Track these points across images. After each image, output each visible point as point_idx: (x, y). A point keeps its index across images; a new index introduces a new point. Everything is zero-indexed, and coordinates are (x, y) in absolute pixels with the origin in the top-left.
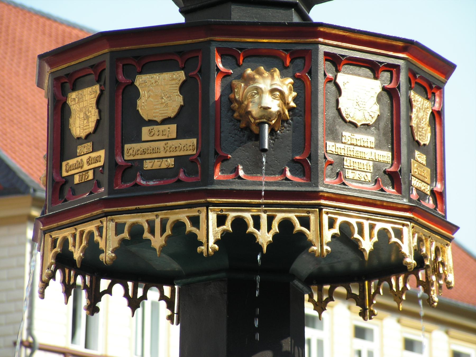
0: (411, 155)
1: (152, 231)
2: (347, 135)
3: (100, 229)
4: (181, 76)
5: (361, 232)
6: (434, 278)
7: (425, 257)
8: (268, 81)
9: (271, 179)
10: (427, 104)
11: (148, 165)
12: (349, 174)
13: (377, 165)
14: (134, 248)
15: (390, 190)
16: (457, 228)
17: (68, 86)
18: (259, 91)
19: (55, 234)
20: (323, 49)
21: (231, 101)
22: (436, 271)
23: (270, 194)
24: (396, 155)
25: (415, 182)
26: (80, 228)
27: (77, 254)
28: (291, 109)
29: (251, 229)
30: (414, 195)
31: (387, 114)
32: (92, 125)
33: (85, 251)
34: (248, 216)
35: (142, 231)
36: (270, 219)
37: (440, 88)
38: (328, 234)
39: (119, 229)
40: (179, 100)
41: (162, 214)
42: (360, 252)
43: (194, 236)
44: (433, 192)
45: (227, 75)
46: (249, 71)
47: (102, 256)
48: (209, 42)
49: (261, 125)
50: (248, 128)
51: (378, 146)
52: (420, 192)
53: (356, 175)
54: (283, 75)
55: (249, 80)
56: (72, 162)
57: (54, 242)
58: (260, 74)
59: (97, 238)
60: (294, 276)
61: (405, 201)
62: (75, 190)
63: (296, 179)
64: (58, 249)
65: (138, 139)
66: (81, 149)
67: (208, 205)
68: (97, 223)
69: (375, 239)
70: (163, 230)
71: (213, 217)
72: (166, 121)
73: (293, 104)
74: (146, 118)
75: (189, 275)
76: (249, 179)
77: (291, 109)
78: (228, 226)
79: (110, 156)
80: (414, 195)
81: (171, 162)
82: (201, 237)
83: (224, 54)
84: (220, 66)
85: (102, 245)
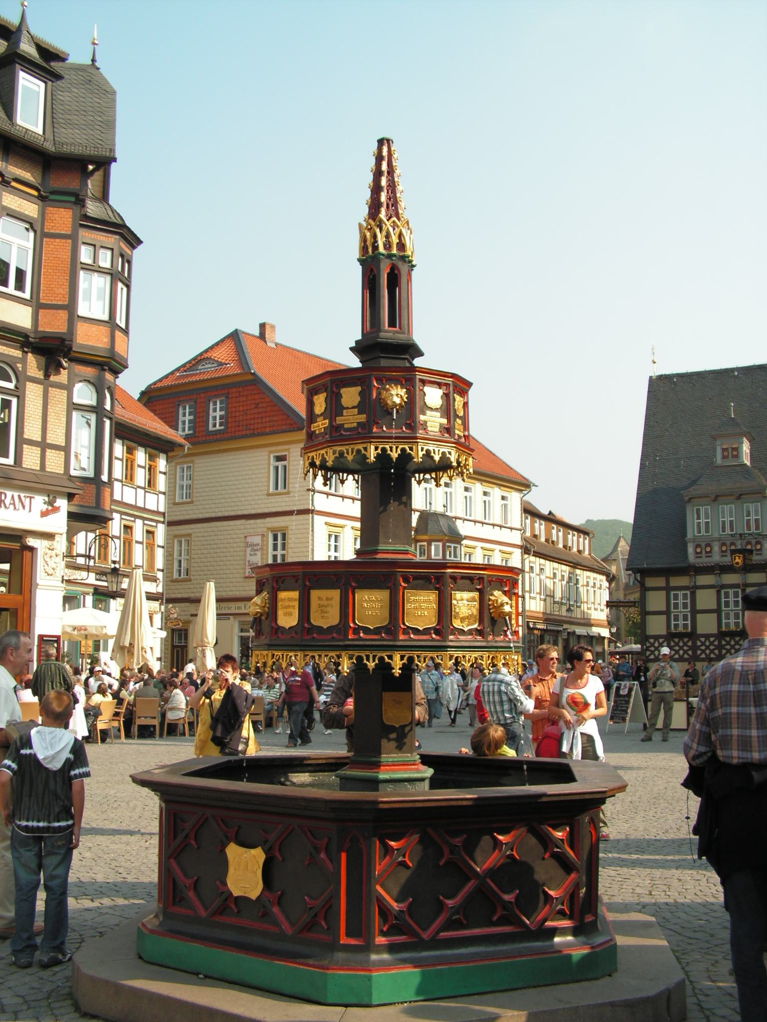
0: (455, 420)
1: (348, 453)
2: (428, 413)
3: (326, 453)
4: (359, 388)
5: (434, 453)
6: (465, 471)
7: (461, 462)
8: (395, 391)
9: (397, 431)
10: (462, 399)
11: (346, 426)
12: (429, 429)
13: (441, 425)
14: (342, 460)
15: (447, 435)
16: (140, 242)
17: (314, 393)
18: (392, 395)
19: (309, 454)
20: (418, 377)
21: (380, 399)
22: (465, 468)
23: (396, 438)
24: (449, 421)
25: (457, 432)
26: (319, 452)
27: (318, 463)
28: (405, 402)
29: (389, 452)
30: (456, 437)
31: (445, 404)
32: (323, 409)
33: (321, 461)
34: (388, 447)
35: (344, 453)
36: (397, 448)
37: (467, 392)
38: (421, 454)
39: (334, 453)
40: (359, 399)
41: (352, 446)
42: (435, 461)
43: (365, 455)
44: (464, 436)
45: (378, 388)
46: (388, 386)
47: (327, 464)
48: (371, 375)
49: (392, 409)
50: (387, 410)
51: (441, 417)
52: (460, 437)
53: (433, 429)
54: (402, 388)
55: (387, 390)
56: (315, 424)
57: (309, 457)
58: (392, 387)
59: (325, 456)
60: (407, 471)
61: (453, 440)
62: (317, 436)
63: (408, 431)
64: (310, 461)
65: (342, 415)
66: (318, 419)
67: (371, 442)
68: (325, 450)
69: (440, 455)
70: (352, 453)
71: (373, 447)
72: (353, 407)
73: (406, 400)
74: (345, 406)
75: (365, 470)
76: (388, 431)
77: (405, 402)
78: (379, 451)
79: (330, 423)
80: (456, 437)
81: (355, 425)
82: (368, 456)
83: (377, 379)
84: (376, 384)
85: (327, 459)
